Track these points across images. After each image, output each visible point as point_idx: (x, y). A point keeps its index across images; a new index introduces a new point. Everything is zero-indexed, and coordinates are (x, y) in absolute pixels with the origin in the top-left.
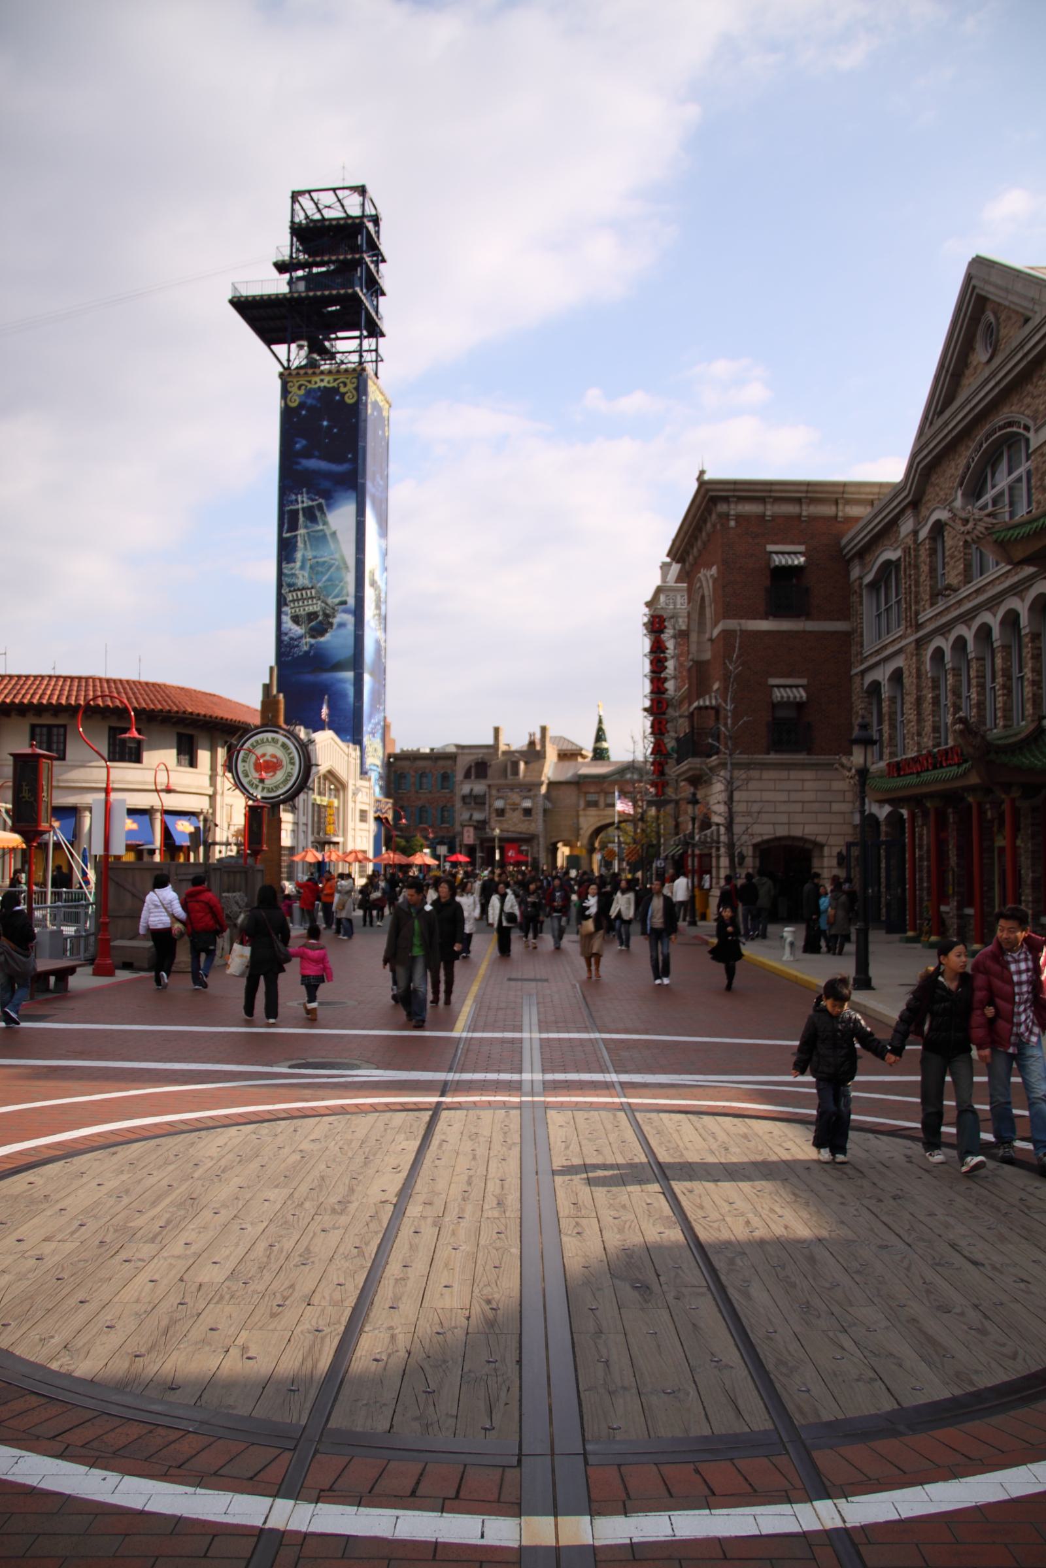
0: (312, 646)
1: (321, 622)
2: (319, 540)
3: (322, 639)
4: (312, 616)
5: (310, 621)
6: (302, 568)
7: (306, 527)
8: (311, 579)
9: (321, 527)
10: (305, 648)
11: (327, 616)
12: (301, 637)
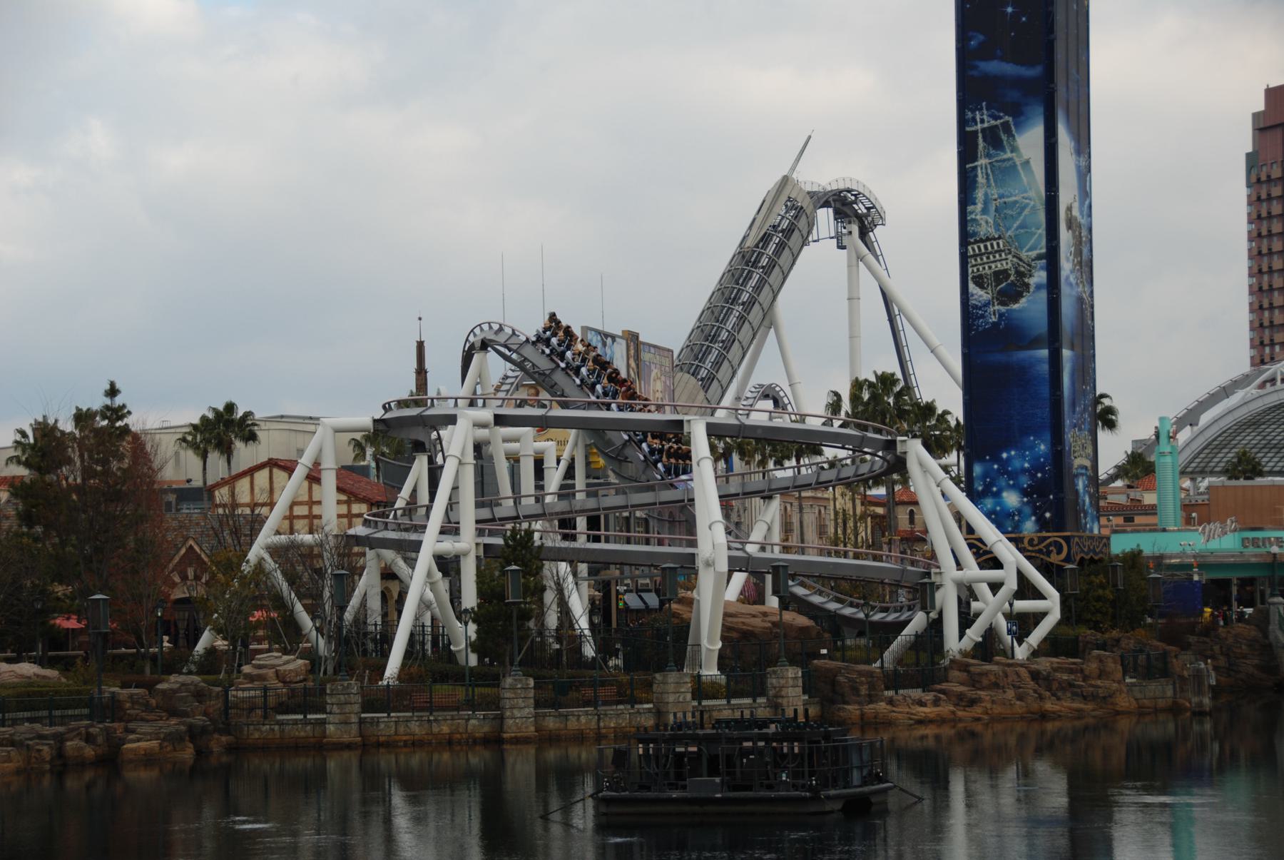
0: (1001, 315)
1: (1013, 283)
2: (1006, 172)
3: (1016, 306)
4: (1000, 276)
5: (998, 282)
6: (985, 211)
7: (988, 156)
8: (997, 226)
9: (1009, 155)
10: (994, 319)
11: (1020, 275)
12: (987, 304)
